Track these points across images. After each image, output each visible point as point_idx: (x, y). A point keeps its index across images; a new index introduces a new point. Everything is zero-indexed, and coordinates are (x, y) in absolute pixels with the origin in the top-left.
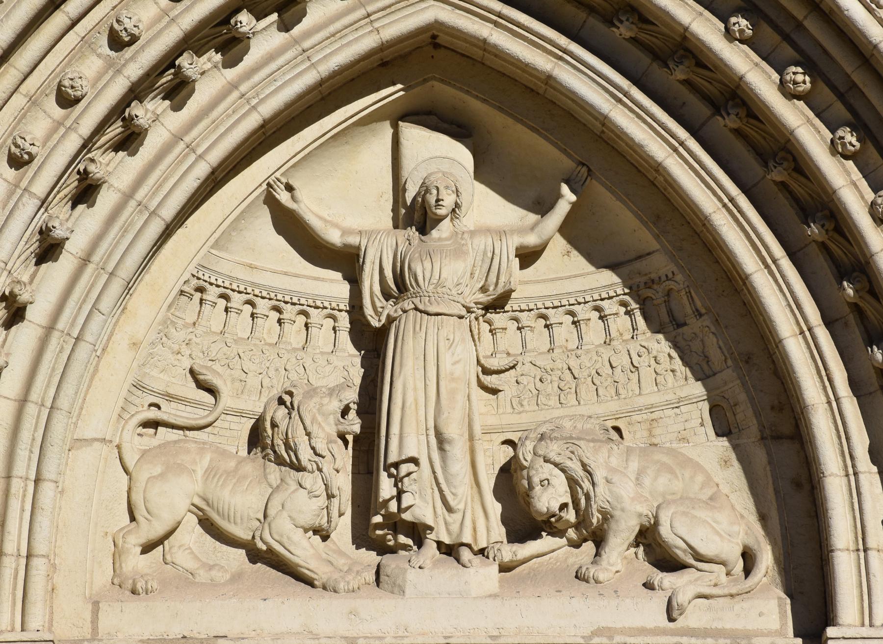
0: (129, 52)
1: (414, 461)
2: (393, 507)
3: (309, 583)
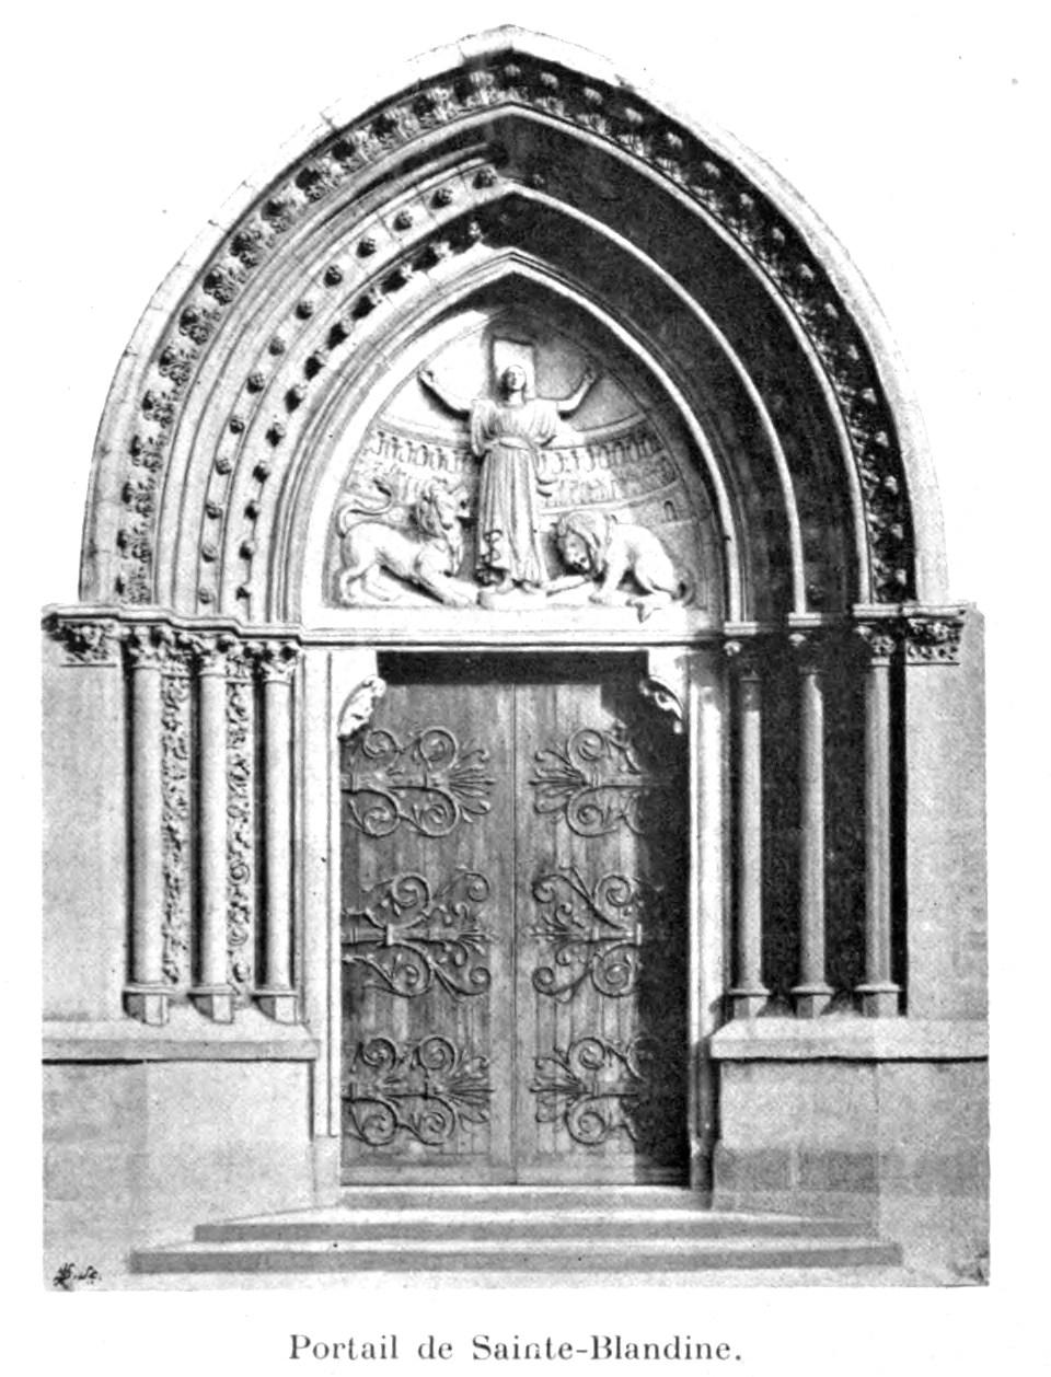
0: (405, 232)
1: (499, 531)
2: (487, 559)
3: (438, 599)
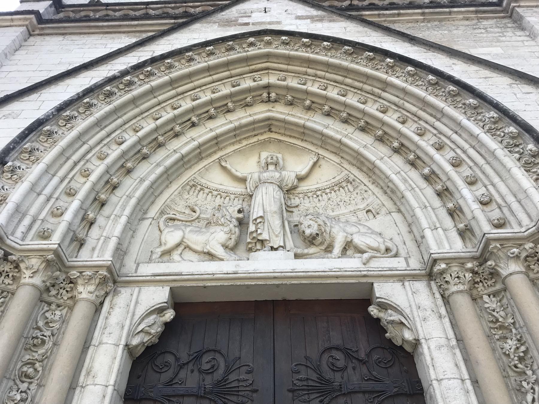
1: (261, 217)
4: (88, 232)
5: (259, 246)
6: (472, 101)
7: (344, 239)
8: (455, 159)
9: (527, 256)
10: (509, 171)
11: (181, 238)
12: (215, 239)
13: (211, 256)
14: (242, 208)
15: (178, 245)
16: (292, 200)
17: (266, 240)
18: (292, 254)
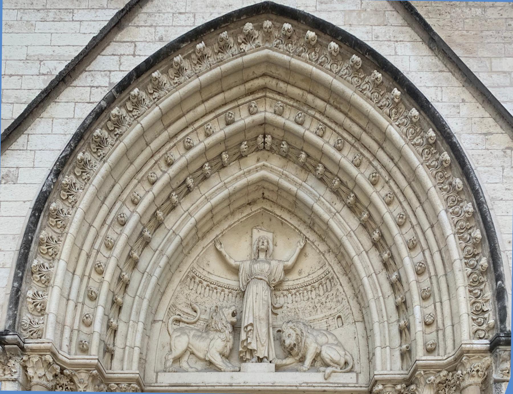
1: (252, 325)
4: (114, 340)
5: (248, 356)
6: (458, 182)
7: (314, 351)
8: (421, 266)
9: (440, 383)
10: (457, 289)
11: (187, 344)
12: (214, 347)
13: (211, 365)
14: (236, 310)
15: (185, 351)
16: (278, 298)
17: (254, 350)
18: (273, 366)
